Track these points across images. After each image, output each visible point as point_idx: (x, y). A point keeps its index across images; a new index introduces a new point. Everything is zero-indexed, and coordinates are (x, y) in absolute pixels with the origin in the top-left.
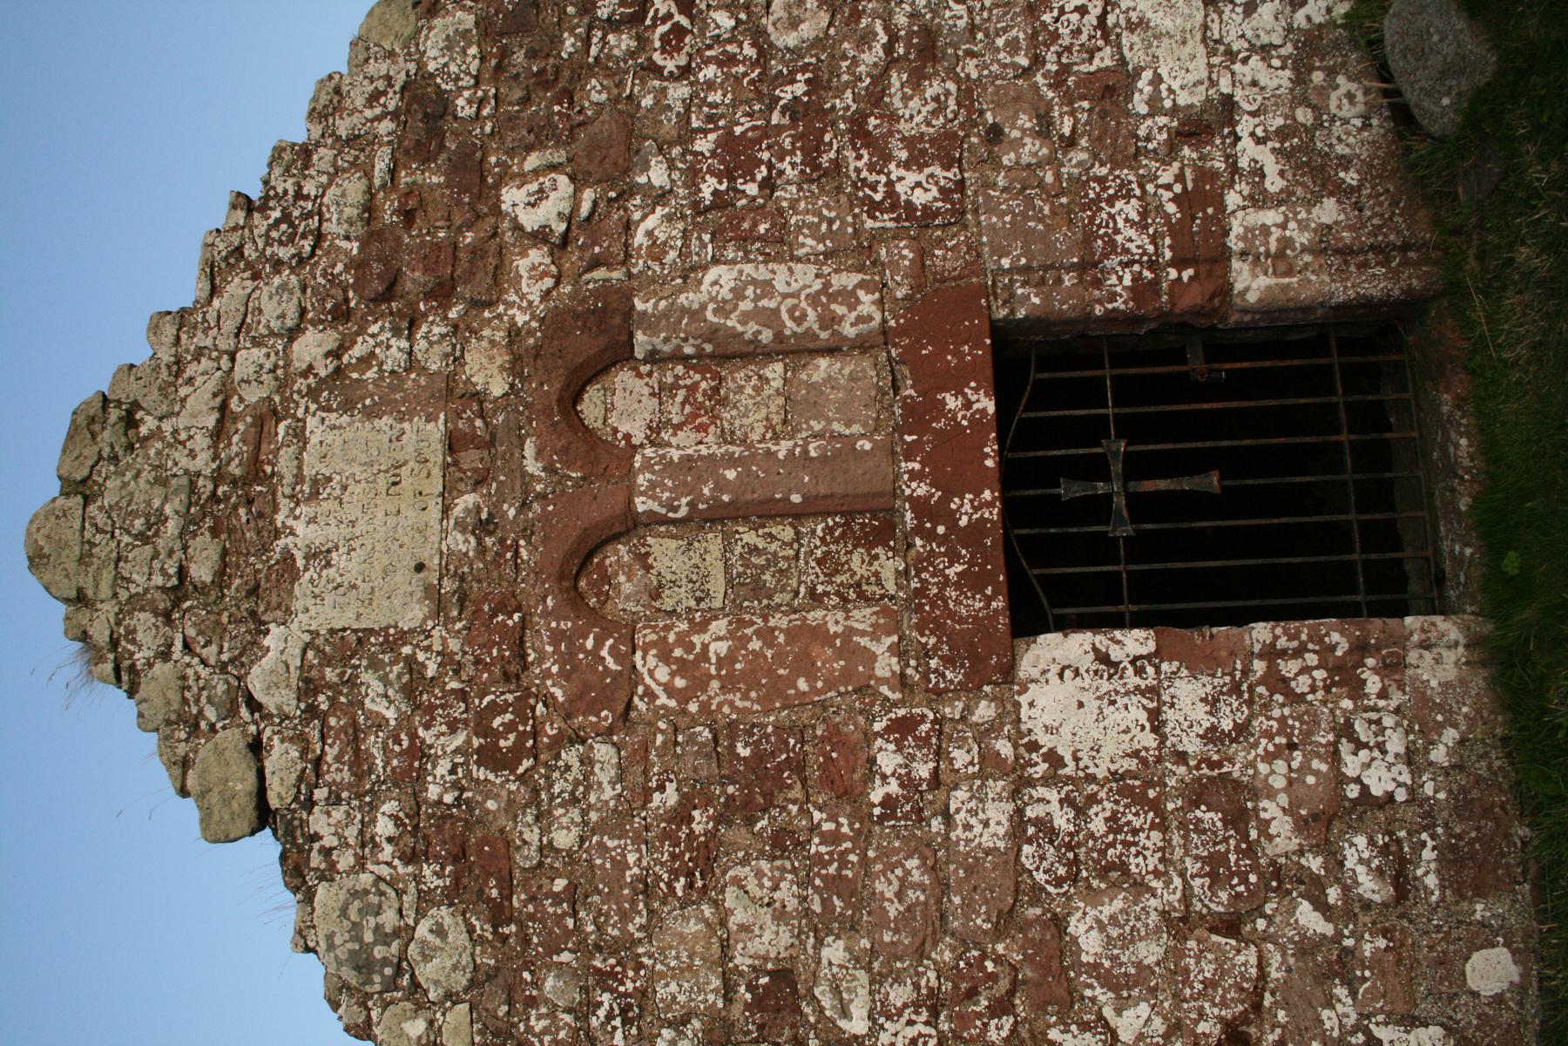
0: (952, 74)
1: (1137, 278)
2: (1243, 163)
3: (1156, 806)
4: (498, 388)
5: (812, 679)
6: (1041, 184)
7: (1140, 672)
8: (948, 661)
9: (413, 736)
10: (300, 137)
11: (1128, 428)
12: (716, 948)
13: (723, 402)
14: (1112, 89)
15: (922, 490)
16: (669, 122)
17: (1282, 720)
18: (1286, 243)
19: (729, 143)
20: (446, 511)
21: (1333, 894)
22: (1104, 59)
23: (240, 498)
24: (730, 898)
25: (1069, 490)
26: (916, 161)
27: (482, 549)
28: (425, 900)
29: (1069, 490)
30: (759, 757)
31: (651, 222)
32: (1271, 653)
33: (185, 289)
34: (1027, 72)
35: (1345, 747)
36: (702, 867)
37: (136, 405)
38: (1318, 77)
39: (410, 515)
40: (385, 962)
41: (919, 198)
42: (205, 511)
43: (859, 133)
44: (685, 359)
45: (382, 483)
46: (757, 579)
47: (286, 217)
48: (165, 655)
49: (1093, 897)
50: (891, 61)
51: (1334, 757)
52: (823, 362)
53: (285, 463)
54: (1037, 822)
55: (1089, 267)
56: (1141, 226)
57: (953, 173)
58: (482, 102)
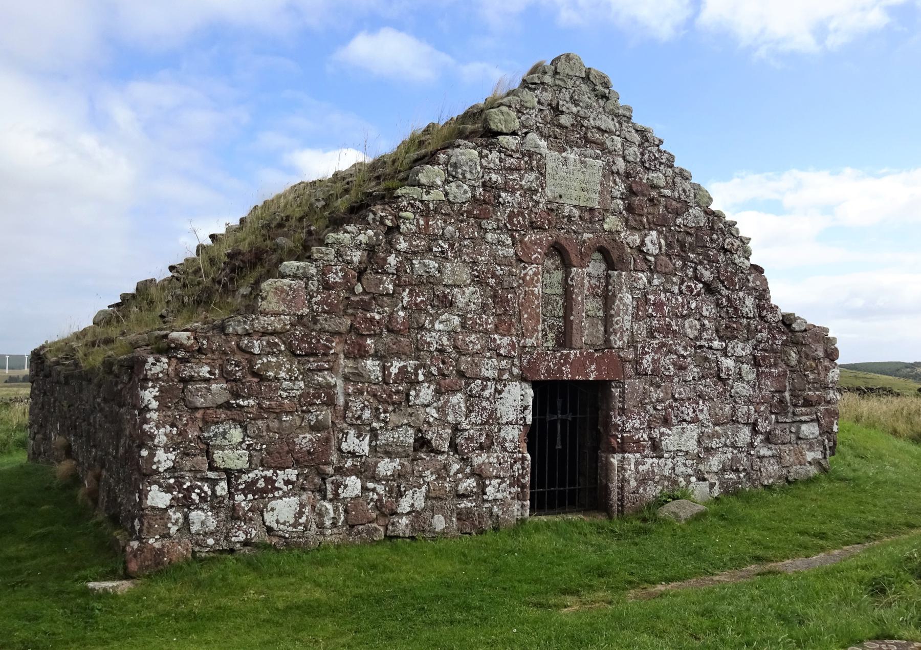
0: (675, 374)
1: (619, 425)
2: (646, 460)
3: (487, 423)
4: (606, 226)
5: (527, 319)
6: (645, 398)
7: (521, 419)
8: (529, 362)
9: (518, 190)
10: (676, 164)
11: (574, 419)
12: (458, 283)
13: (594, 297)
14: (666, 422)
15: (572, 357)
16: (668, 286)
17: (507, 462)
18: (625, 470)
19: (662, 304)
20: (575, 206)
21: (460, 476)
22: (674, 421)
23: (581, 137)
24: (471, 289)
25: (559, 404)
26: (654, 361)
27: (563, 217)
28: (473, 188)
29: (559, 404)
30: (508, 301)
31: (644, 279)
32: (524, 459)
33: (639, 120)
34: (673, 396)
35: (499, 481)
36: (479, 281)
37: (608, 99)
38: (666, 483)
39: (575, 194)
40: (457, 173)
41: (645, 361)
42: (579, 122)
43: (663, 345)
44: (607, 286)
45: (584, 185)
46: (550, 303)
47: (656, 158)
48: (539, 102)
49: (466, 401)
50: (679, 356)
51: (497, 477)
52: (602, 329)
53: (589, 151)
54: (486, 386)
55: (623, 411)
56: (633, 428)
57: (650, 372)
58: (679, 227)
